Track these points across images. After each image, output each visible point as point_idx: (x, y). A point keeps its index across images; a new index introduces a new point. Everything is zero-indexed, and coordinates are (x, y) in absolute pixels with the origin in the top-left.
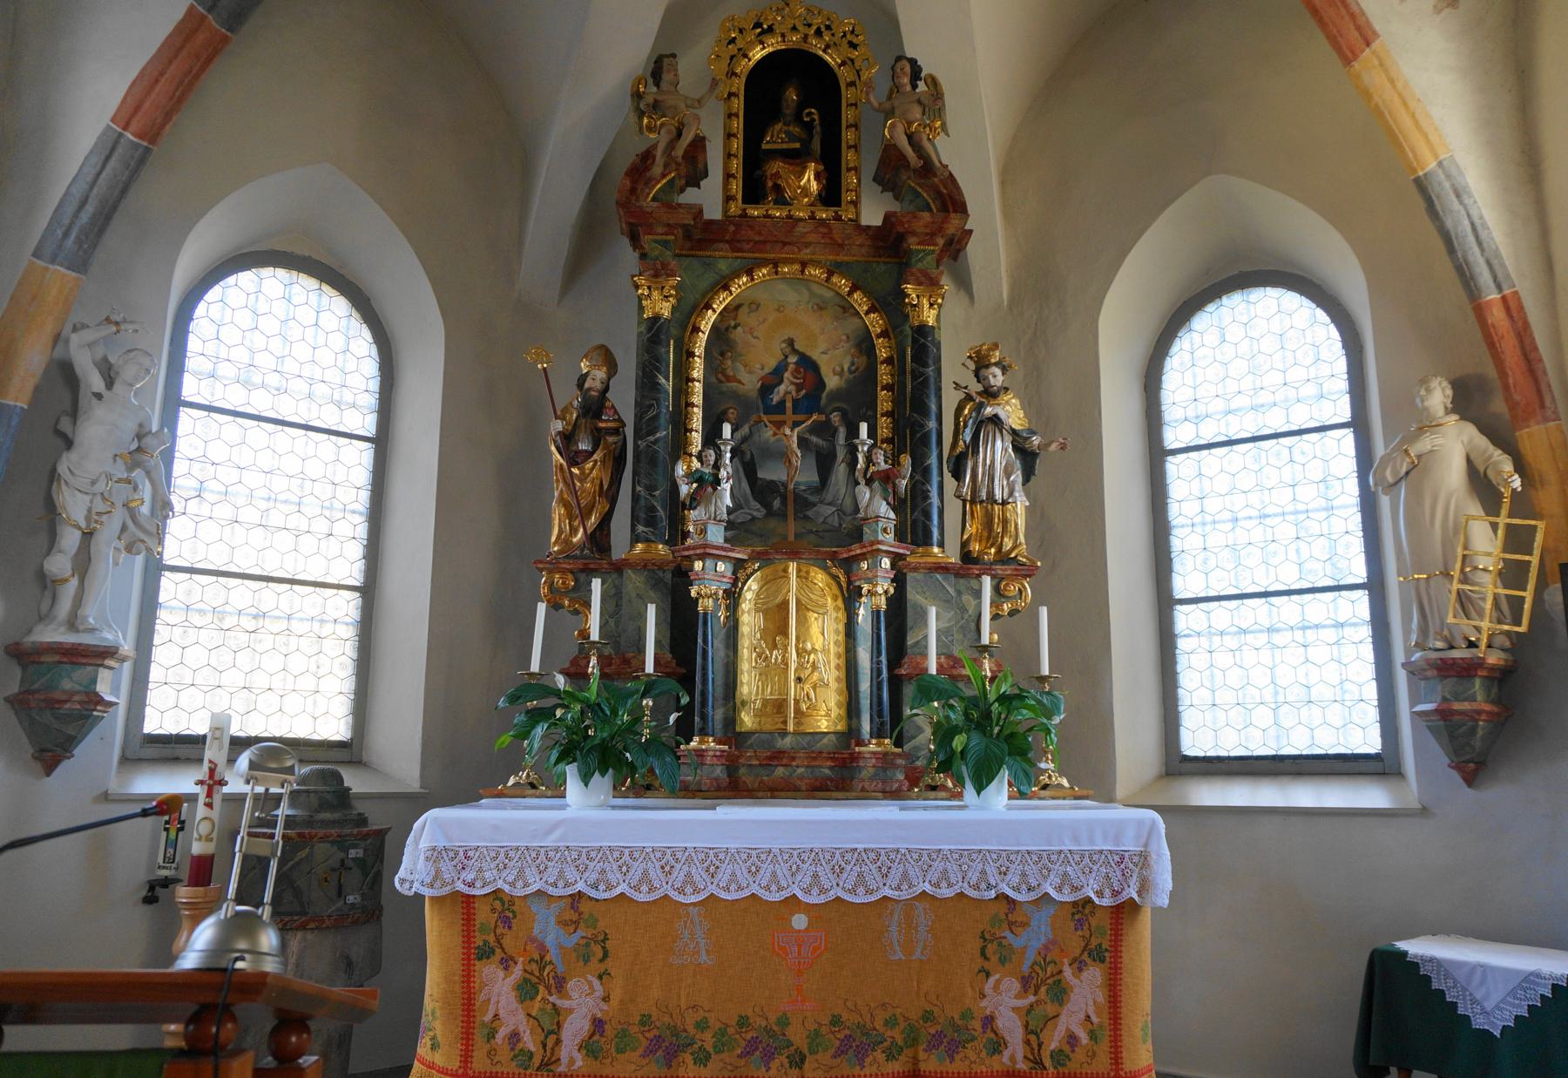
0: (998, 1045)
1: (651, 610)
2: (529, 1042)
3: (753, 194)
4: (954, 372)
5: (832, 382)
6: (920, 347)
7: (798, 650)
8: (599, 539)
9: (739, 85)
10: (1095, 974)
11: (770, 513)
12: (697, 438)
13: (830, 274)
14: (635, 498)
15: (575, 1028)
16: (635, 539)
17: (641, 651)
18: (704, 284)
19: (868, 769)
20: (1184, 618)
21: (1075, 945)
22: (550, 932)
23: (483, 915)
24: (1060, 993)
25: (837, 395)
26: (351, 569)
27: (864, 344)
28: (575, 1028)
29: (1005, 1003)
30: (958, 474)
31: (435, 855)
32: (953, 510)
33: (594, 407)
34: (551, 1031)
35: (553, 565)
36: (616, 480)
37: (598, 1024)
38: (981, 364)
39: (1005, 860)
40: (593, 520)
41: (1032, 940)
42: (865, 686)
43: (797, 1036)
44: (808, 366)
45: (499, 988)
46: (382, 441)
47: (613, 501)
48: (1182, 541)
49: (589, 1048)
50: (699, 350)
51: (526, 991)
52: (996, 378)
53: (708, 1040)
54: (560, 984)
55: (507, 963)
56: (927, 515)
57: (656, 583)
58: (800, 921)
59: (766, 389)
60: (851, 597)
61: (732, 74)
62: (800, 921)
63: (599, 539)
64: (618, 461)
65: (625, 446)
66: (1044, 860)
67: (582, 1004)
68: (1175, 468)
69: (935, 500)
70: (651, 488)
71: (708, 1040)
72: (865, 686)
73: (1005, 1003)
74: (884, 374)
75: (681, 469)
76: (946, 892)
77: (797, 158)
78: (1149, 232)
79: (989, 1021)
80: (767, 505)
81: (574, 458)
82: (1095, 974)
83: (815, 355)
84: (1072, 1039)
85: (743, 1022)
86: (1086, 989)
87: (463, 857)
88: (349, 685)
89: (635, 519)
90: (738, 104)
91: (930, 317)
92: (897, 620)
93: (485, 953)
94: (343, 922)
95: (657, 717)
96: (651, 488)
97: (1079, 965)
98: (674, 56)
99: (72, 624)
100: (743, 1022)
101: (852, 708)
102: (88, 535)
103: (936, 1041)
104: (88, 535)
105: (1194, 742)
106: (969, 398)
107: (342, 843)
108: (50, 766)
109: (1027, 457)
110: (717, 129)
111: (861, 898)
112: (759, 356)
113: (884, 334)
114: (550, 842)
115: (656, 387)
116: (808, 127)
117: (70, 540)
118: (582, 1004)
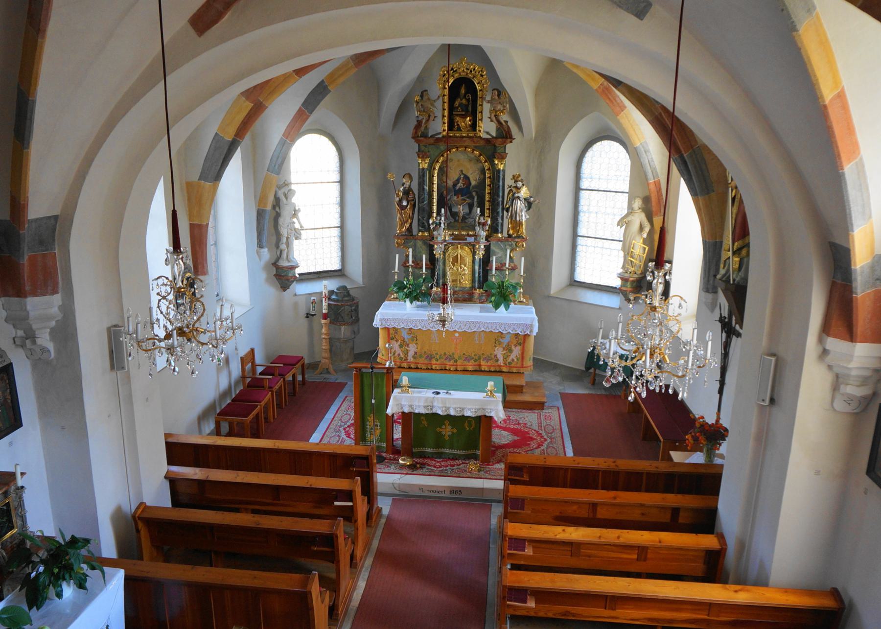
0: (497, 360)
1: (424, 256)
2: (402, 356)
3: (451, 128)
4: (509, 182)
5: (473, 183)
6: (497, 176)
7: (461, 270)
8: (410, 230)
9: (446, 92)
10: (519, 348)
11: (456, 221)
12: (435, 215)
13: (474, 150)
14: (419, 220)
15: (411, 354)
16: (419, 231)
17: (422, 261)
18: (437, 154)
19: (476, 296)
20: (580, 241)
21: (515, 342)
22: (405, 334)
23: (391, 331)
24: (511, 351)
25: (475, 187)
26: (336, 222)
27: (483, 172)
28: (411, 354)
29: (499, 352)
30: (507, 211)
31: (381, 320)
32: (506, 221)
33: (407, 192)
34: (406, 354)
35: (398, 237)
36: (413, 214)
37: (416, 353)
38: (516, 179)
39: (500, 324)
40: (407, 225)
41: (505, 341)
42: (477, 275)
43: (456, 357)
44: (466, 178)
45: (396, 345)
46: (342, 182)
47: (412, 219)
48: (583, 218)
49: (414, 357)
50: (435, 182)
51: (401, 346)
52: (520, 184)
53: (438, 357)
54: (408, 345)
55: (397, 341)
56: (497, 225)
57: (425, 243)
58: (457, 335)
59: (455, 185)
60: (474, 253)
61: (444, 88)
62: (457, 335)
63: (410, 230)
64: (414, 206)
65: (417, 203)
66: (510, 325)
67: (412, 349)
68: (583, 194)
69: (500, 221)
70: (423, 218)
71: (438, 357)
72: (477, 275)
73: (499, 352)
74: (488, 182)
75: (431, 221)
76: (487, 330)
77: (464, 117)
78: (571, 131)
79: (496, 356)
80: (454, 218)
81: (403, 208)
82: (519, 348)
83: (469, 175)
84: (513, 360)
85: (445, 354)
86: (516, 351)
87: (387, 320)
88: (339, 254)
89: (419, 225)
90: (446, 98)
91: (501, 167)
92: (486, 261)
93: (392, 339)
94: (352, 323)
95: (427, 286)
96: (423, 218)
97: (516, 346)
98: (426, 91)
99: (288, 260)
100: (445, 354)
101: (473, 281)
102: (288, 238)
103: (484, 359)
104: (288, 238)
105: (582, 276)
106: (511, 190)
107: (351, 306)
108: (284, 291)
109: (529, 205)
110: (440, 109)
111: (470, 331)
112: (453, 175)
113: (489, 169)
114: (405, 318)
115: (424, 189)
116: (468, 100)
117: (284, 240)
118: (412, 349)
